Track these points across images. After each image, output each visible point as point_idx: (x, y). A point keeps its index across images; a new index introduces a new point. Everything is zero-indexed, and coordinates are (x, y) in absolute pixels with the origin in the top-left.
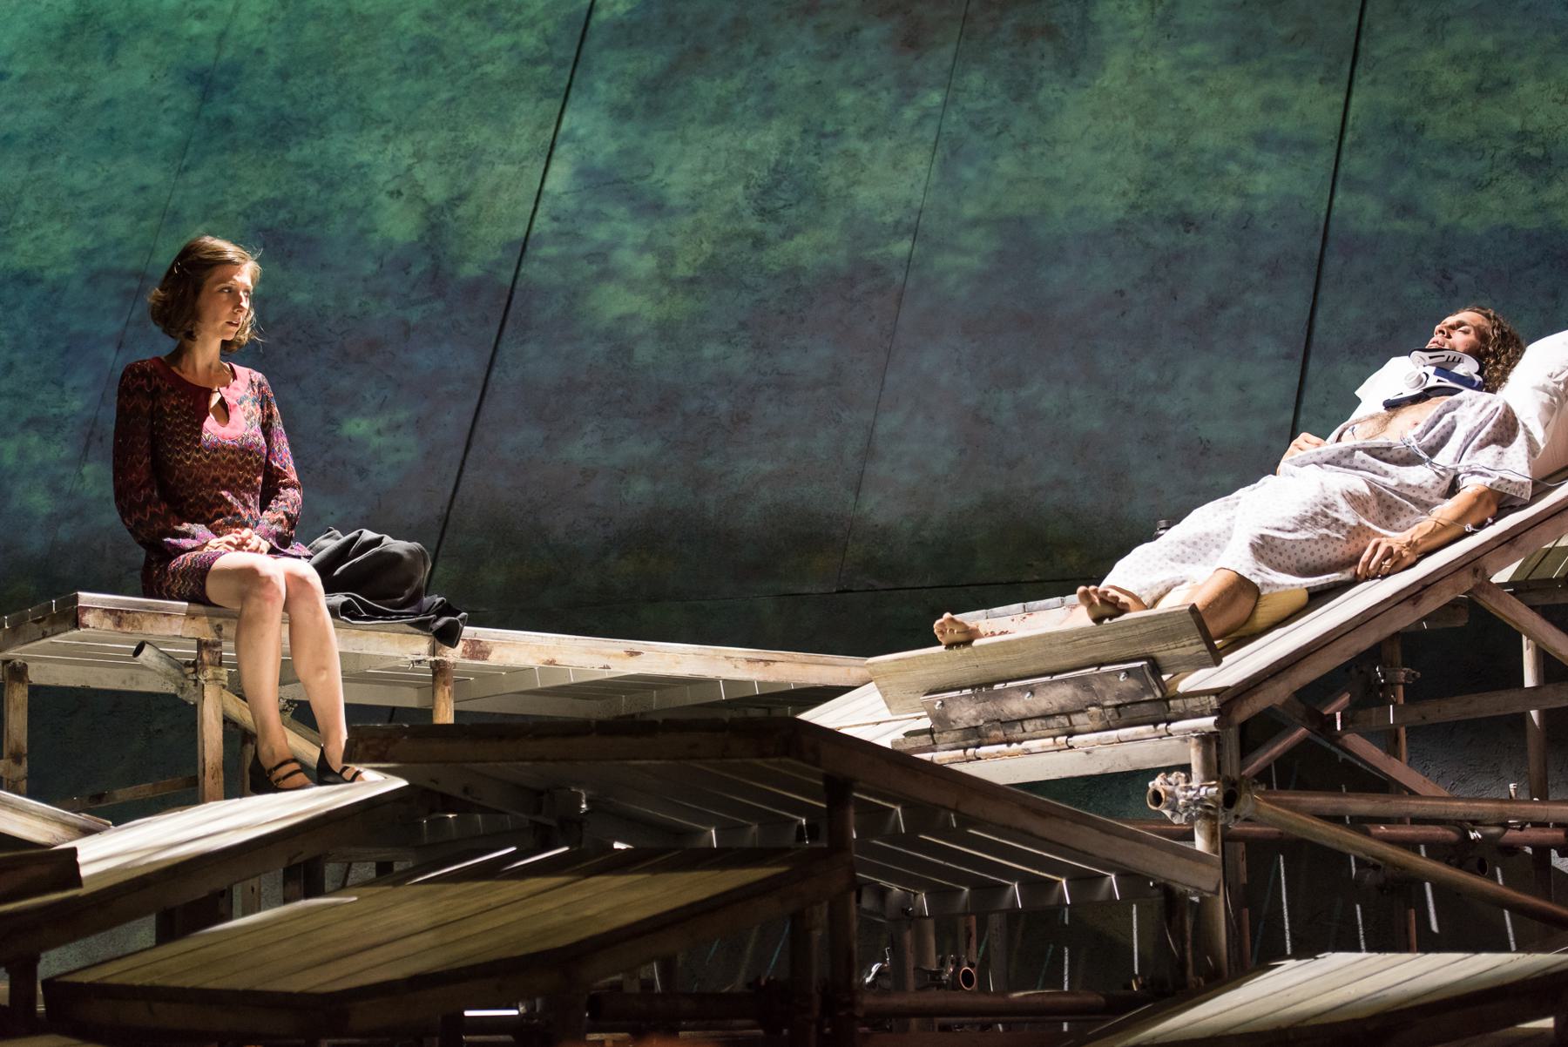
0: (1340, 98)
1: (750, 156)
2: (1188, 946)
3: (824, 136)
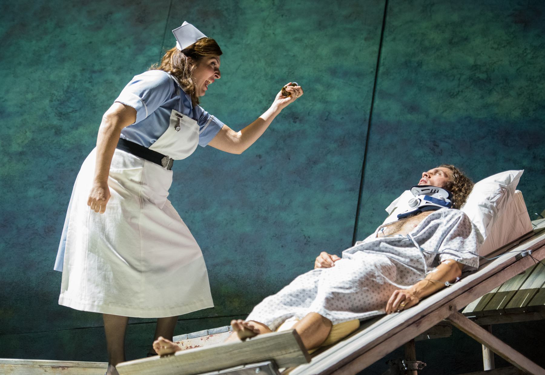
0: (376, 48)
1: (52, 83)
3: (94, 72)
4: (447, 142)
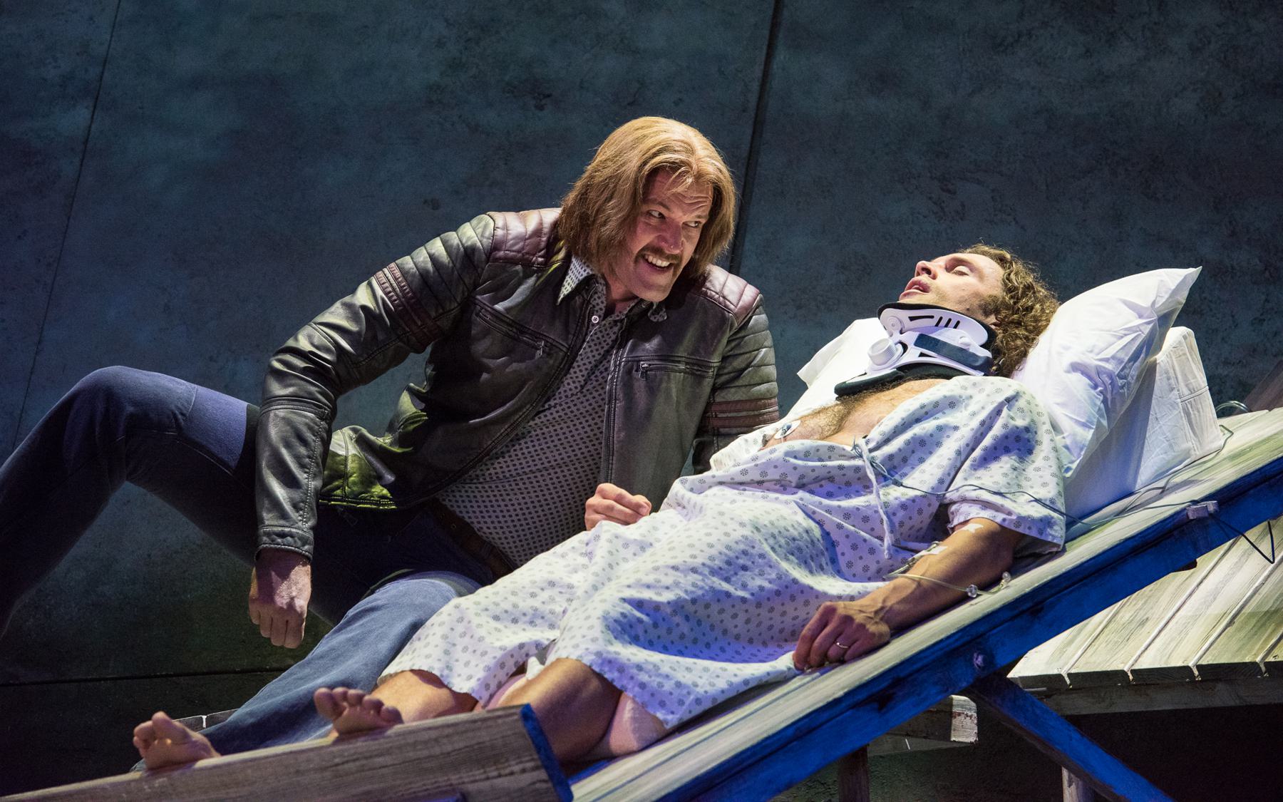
4: (979, 182)
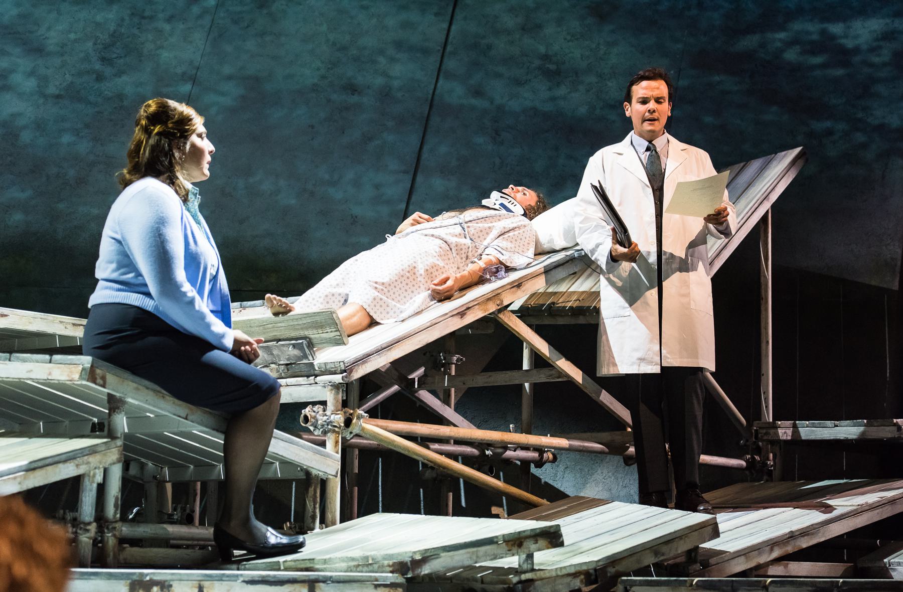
2: (318, 506)
